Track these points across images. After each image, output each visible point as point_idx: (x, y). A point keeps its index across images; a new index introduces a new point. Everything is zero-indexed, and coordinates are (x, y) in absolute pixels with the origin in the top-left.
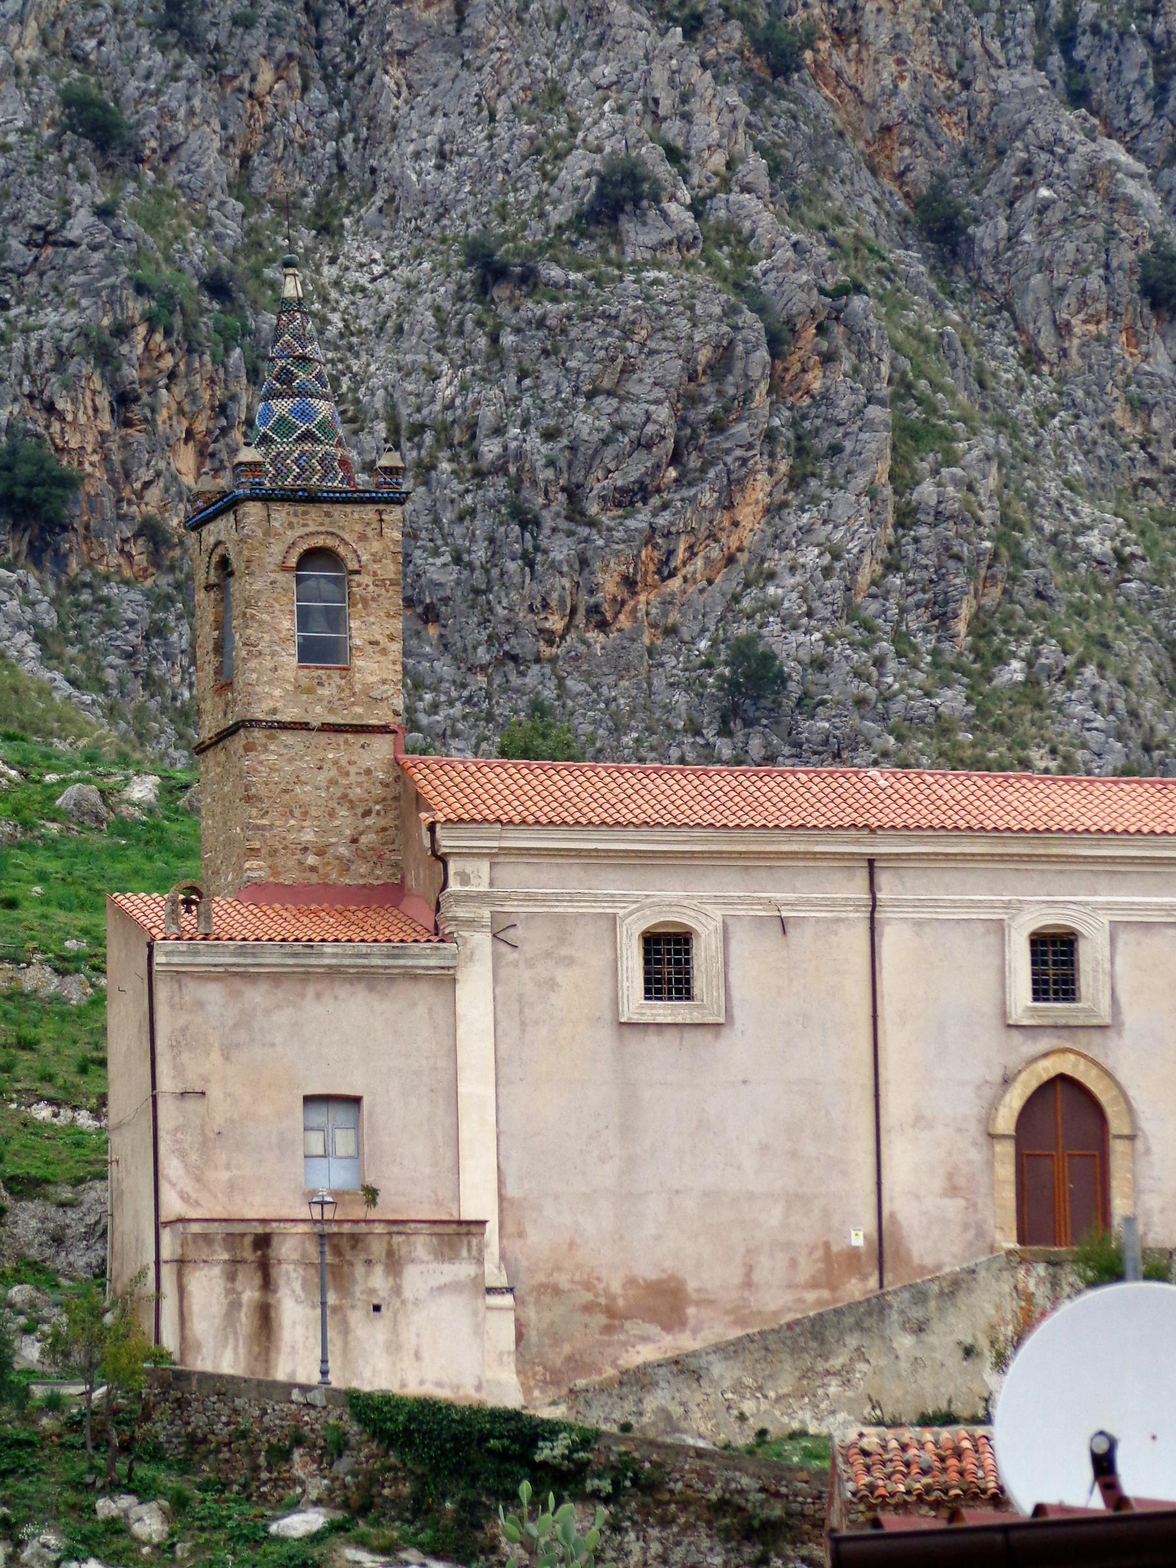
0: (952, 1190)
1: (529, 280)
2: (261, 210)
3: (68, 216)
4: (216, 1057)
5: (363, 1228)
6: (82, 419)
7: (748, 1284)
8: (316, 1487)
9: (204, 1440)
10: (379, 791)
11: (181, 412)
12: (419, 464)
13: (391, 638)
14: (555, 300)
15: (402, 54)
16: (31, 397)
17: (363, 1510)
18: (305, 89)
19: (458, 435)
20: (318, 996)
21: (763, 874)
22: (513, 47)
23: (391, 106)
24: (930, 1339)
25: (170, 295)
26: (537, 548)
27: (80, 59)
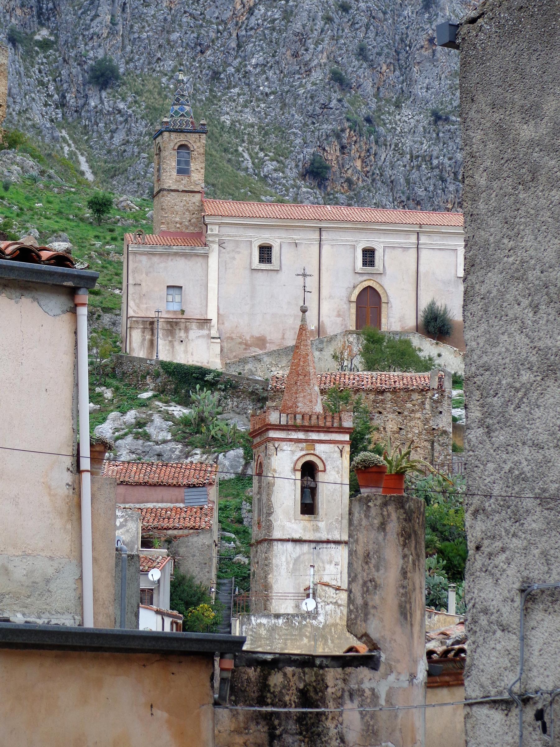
0: (339, 316)
1: (447, 120)
2: (382, 101)
3: (331, 101)
4: (144, 275)
5: (179, 320)
6: (332, 152)
7: (283, 338)
8: (152, 386)
9: (126, 373)
10: (197, 208)
11: (358, 151)
12: (417, 165)
13: (202, 168)
14: (453, 125)
15: (419, 63)
16: (319, 146)
17: (162, 392)
18: (394, 71)
19: (427, 158)
20: (172, 260)
21: (291, 231)
22: (446, 62)
23: (415, 76)
24: (324, 353)
25: (356, 122)
26: (446, 187)
27: (337, 62)
